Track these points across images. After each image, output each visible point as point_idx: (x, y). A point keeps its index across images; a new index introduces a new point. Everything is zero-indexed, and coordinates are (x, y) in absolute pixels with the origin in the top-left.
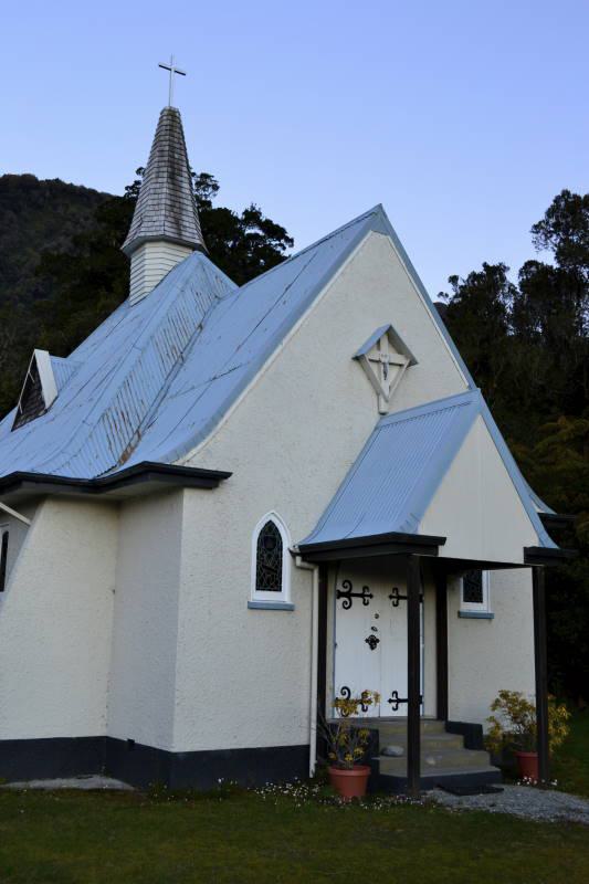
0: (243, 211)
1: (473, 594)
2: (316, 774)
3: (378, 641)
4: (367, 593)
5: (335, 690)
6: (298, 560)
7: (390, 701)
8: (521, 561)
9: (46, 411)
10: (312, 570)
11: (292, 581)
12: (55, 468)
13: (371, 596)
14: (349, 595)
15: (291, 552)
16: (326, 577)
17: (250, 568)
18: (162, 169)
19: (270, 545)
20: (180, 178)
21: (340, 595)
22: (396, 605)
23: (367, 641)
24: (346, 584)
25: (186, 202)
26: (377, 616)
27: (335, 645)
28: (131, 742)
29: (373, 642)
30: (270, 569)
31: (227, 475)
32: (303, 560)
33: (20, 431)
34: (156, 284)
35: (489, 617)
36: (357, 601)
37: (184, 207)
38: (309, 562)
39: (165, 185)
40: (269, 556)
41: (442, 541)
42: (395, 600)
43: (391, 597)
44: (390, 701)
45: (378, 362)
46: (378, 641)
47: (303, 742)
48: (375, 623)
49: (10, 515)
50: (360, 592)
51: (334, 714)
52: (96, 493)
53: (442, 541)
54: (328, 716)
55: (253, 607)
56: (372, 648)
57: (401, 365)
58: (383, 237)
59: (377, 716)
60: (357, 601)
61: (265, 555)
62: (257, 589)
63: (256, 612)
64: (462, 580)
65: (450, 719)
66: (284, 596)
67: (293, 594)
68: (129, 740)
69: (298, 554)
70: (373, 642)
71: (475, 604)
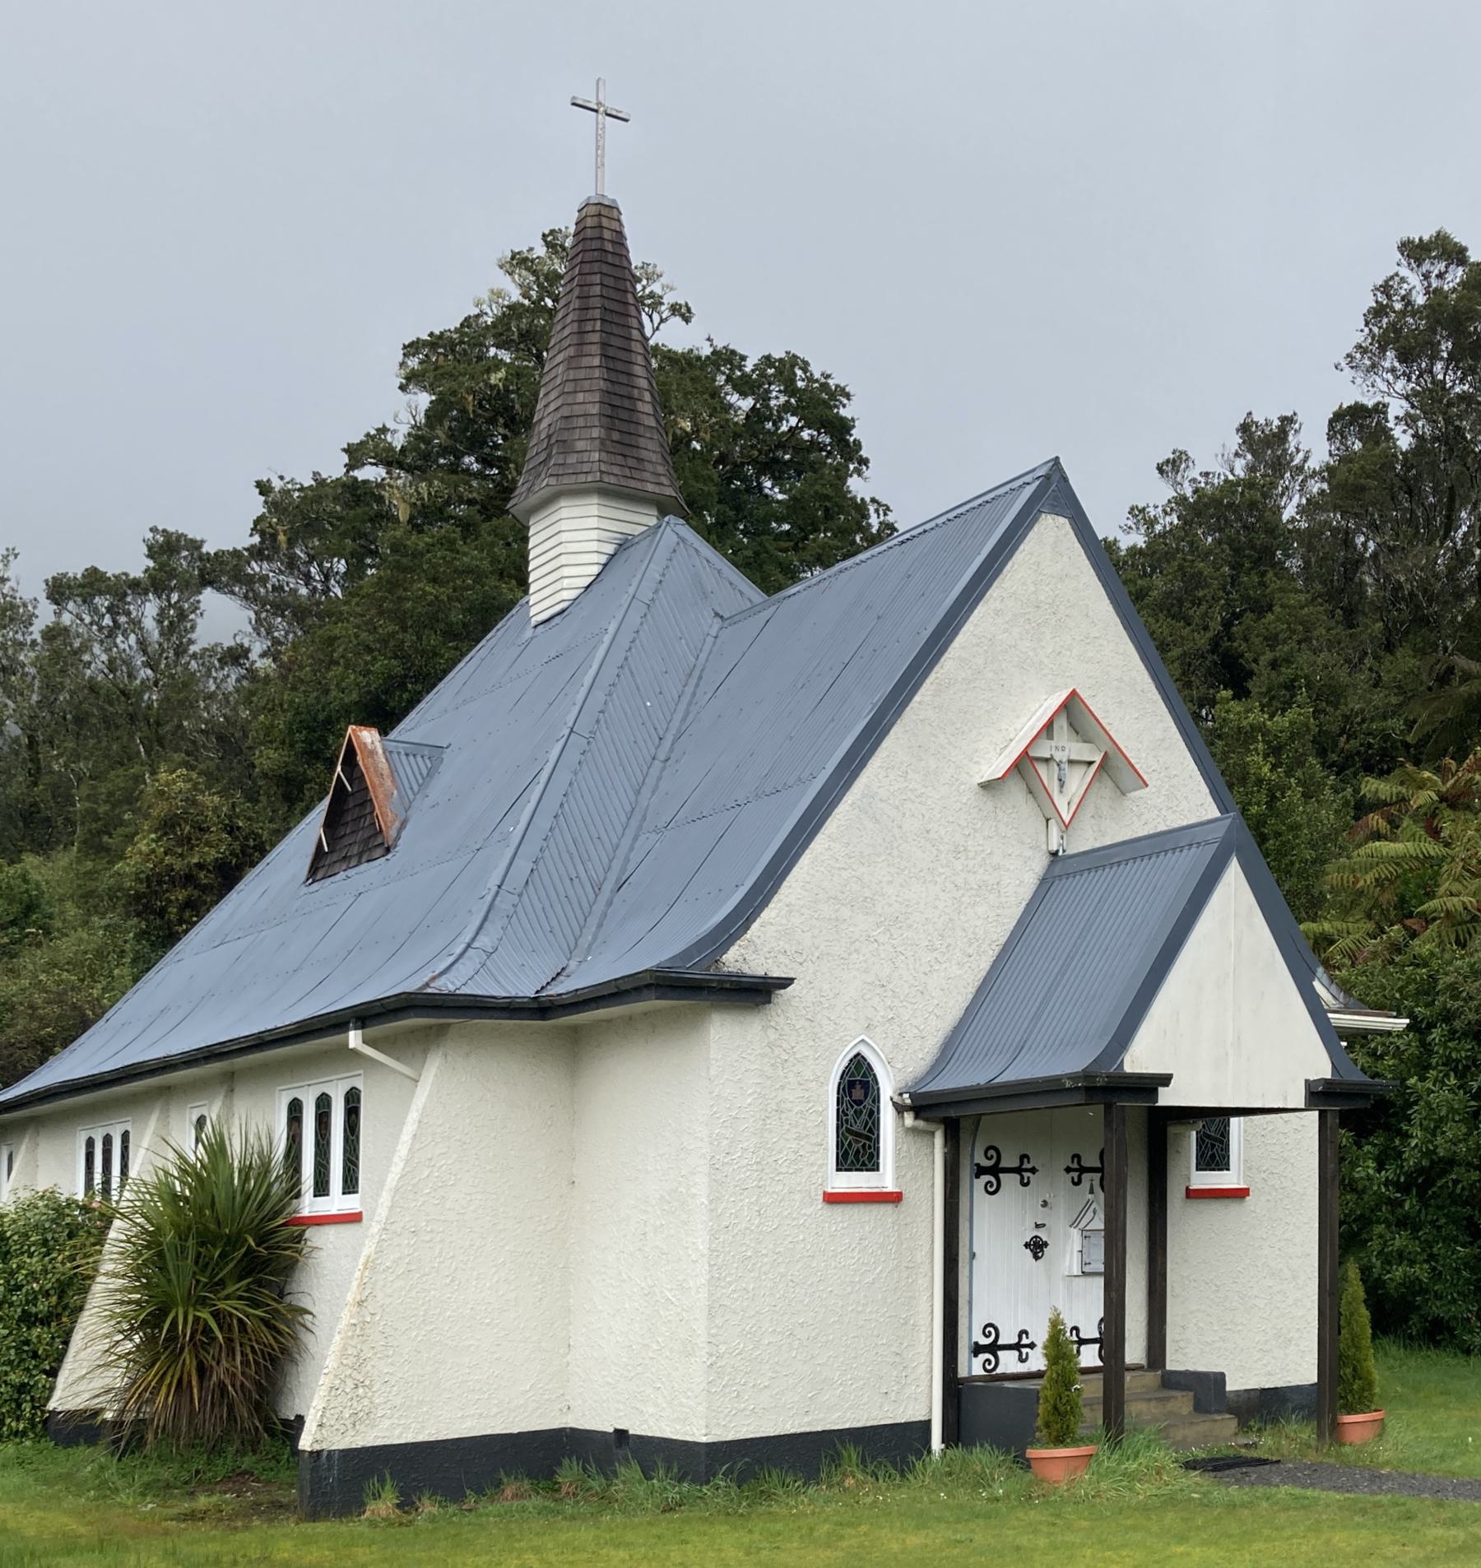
1: (1212, 1156)
3: (1046, 1244)
4: (1026, 1166)
5: (972, 1332)
6: (909, 1119)
7: (1032, 1346)
9: (388, 850)
10: (933, 1134)
11: (898, 1152)
12: (458, 984)
13: (1033, 1170)
14: (995, 1171)
15: (895, 1104)
16: (958, 1142)
17: (826, 1136)
19: (858, 1093)
21: (980, 1171)
22: (1077, 1183)
23: (1027, 1245)
24: (991, 1152)
26: (1045, 1204)
27: (973, 1256)
28: (621, 1434)
29: (1037, 1247)
31: (786, 982)
32: (916, 1117)
33: (326, 887)
34: (587, 581)
35: (1240, 1194)
36: (1009, 1181)
38: (926, 1120)
39: (597, 373)
40: (858, 1113)
41: (1165, 1080)
43: (1068, 1170)
46: (1046, 1244)
47: (918, 1415)
49: (382, 1064)
50: (1015, 1164)
51: (973, 1367)
52: (543, 1019)
53: (1165, 1080)
54: (962, 1372)
55: (832, 1199)
56: (1036, 1258)
57: (1090, 763)
60: (1009, 1181)
61: (851, 1112)
62: (838, 1170)
64: (1194, 1133)
65: (1170, 1366)
66: (885, 1179)
67: (898, 1177)
68: (617, 1431)
70: (1037, 1247)
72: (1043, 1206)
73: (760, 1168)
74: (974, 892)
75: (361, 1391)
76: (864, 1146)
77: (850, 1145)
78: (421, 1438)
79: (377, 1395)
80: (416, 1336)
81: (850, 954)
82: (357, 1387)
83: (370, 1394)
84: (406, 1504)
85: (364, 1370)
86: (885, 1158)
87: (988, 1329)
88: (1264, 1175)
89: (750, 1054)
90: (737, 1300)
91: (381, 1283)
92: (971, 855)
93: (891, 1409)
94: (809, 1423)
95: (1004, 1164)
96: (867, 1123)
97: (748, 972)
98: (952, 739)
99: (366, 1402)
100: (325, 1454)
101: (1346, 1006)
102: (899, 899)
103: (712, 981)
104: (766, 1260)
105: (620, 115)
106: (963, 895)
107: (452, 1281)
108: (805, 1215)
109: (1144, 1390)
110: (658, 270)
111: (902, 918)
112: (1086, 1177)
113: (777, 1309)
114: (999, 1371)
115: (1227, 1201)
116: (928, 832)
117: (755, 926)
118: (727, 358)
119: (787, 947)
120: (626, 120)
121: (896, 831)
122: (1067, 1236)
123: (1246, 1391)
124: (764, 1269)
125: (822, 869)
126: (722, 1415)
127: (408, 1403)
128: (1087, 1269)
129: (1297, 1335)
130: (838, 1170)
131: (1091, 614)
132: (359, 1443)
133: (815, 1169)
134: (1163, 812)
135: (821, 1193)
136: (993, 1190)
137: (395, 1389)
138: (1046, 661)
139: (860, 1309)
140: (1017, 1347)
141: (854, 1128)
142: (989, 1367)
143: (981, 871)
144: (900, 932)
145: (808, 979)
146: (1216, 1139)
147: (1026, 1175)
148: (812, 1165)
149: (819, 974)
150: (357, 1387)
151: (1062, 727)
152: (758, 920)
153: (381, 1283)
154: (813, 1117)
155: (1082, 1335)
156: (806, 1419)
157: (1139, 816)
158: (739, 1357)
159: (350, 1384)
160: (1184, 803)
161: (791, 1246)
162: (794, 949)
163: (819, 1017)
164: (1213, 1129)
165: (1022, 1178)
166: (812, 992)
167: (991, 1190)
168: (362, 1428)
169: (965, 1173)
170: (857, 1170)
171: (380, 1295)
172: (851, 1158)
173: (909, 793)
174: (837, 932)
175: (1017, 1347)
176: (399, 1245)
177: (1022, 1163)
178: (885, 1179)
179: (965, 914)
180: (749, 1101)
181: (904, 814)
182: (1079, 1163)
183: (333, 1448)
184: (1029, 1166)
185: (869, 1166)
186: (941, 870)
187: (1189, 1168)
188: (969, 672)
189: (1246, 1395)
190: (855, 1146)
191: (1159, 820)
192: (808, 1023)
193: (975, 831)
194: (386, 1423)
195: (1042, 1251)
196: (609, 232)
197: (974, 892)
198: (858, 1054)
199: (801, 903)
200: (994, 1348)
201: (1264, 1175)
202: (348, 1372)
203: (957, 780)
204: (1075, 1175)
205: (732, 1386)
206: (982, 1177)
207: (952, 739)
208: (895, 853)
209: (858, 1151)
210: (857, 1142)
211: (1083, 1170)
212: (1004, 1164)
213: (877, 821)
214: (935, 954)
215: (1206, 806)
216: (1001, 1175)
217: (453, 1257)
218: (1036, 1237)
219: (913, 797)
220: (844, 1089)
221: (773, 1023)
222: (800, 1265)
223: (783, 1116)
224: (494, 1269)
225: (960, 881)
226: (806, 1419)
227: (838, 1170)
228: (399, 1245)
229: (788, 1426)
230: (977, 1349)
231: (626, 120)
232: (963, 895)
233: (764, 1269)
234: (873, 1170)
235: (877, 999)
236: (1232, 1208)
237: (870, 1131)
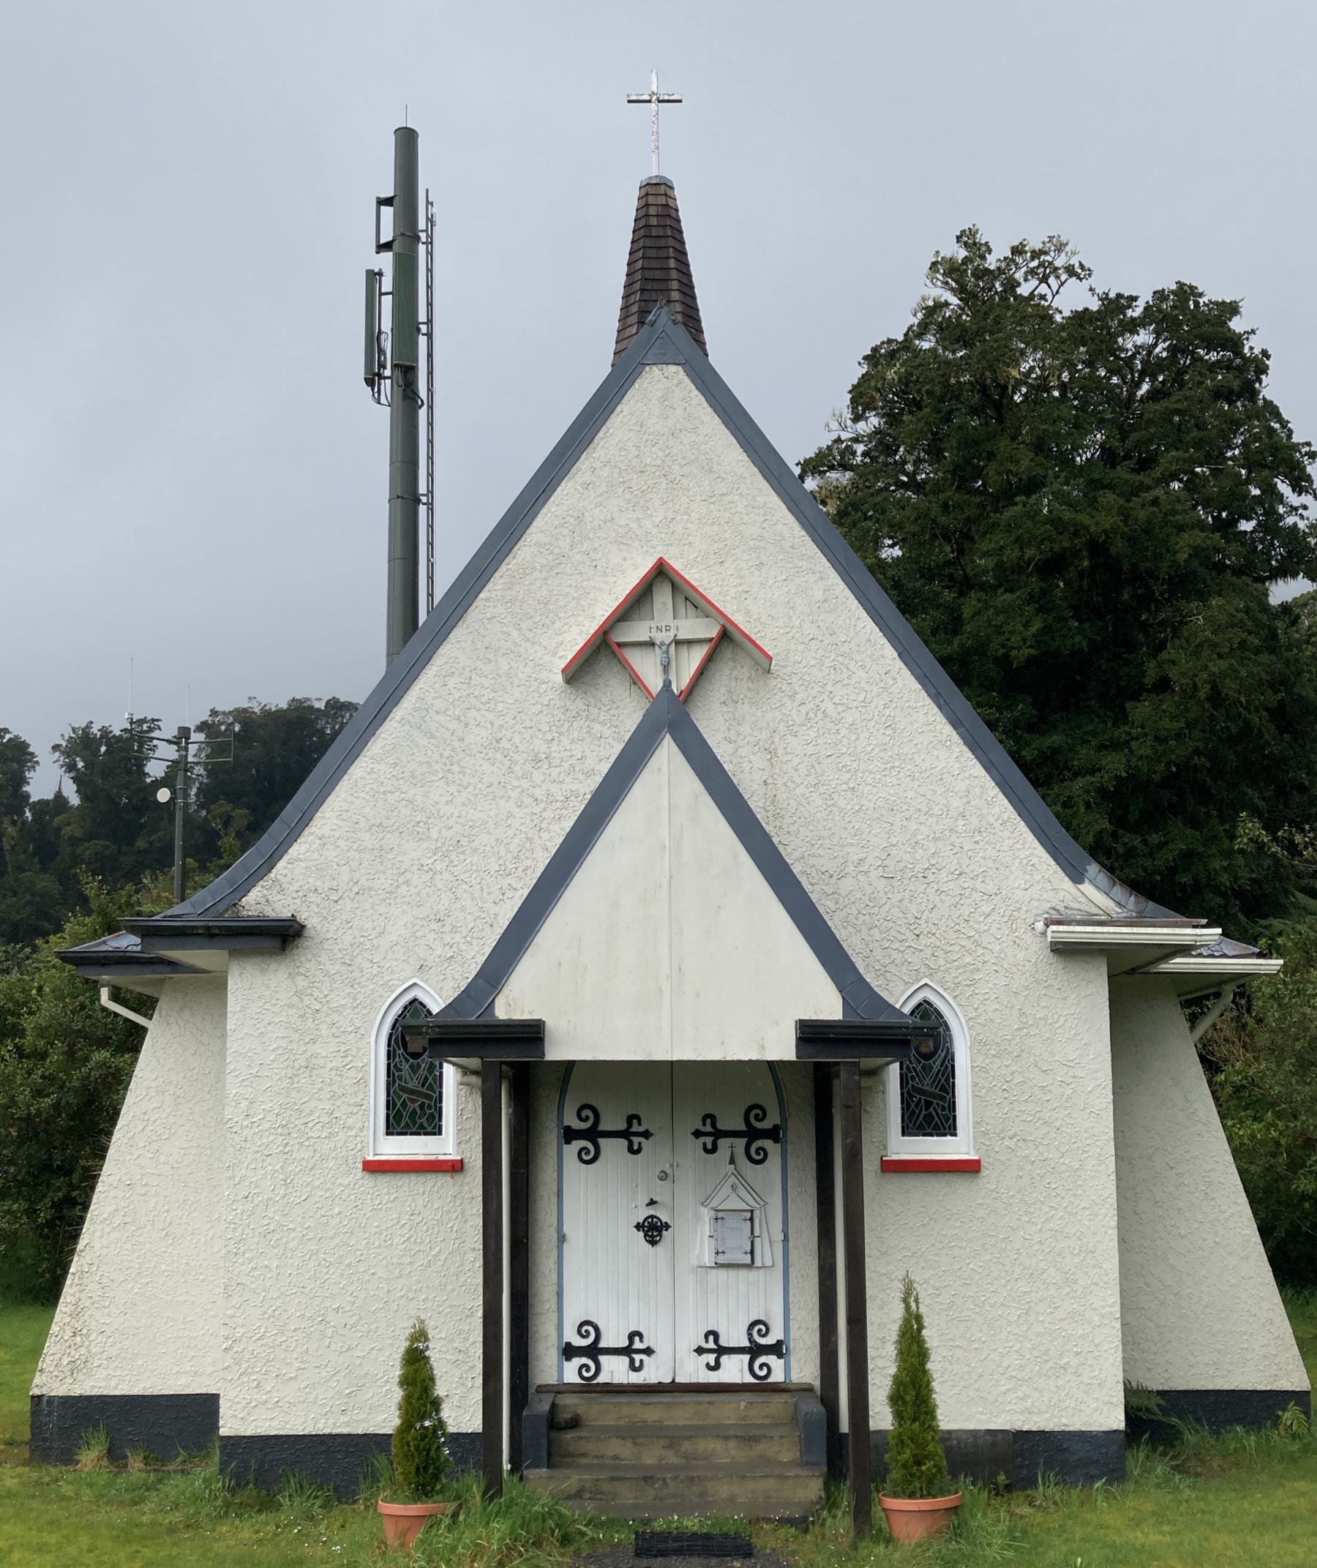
0: (1118, 291)
2: (1145, 1432)
4: (635, 1128)
7: (700, 1351)
13: (646, 1134)
14: (593, 1134)
21: (570, 1135)
22: (713, 1150)
23: (638, 1227)
24: (586, 1113)
27: (562, 1238)
29: (653, 1230)
30: (412, 1092)
35: (970, 1168)
36: (612, 1148)
43: (697, 1134)
44: (648, 1351)
45: (651, 644)
48: (661, 1194)
50: (622, 1126)
55: (375, 1168)
59: (668, 1380)
60: (612, 1148)
63: (385, 1183)
72: (661, 1179)
73: (286, 1131)
74: (559, 804)
75: (78, 1339)
76: (422, 1106)
77: (404, 1104)
78: (135, 1392)
79: (93, 1344)
80: (132, 1288)
81: (397, 887)
82: (75, 1335)
83: (87, 1343)
84: (115, 1455)
85: (82, 1319)
86: (447, 1122)
87: (585, 1328)
88: (1012, 1143)
89: (275, 1005)
90: (257, 1278)
91: (98, 1234)
92: (556, 762)
93: (454, 1415)
94: (347, 1424)
95: (605, 1126)
96: (426, 1079)
97: (272, 915)
98: (530, 635)
99: (83, 1351)
100: (45, 1399)
101: (1141, 914)
102: (462, 820)
103: (196, 927)
104: (293, 1235)
105: (671, 98)
106: (544, 809)
107: (167, 1235)
108: (340, 1185)
109: (768, 1421)
110: (1064, 239)
111: (464, 841)
112: (724, 1143)
113: (306, 1291)
114: (601, 1379)
115: (948, 1177)
116: (498, 741)
117: (281, 864)
118: (1115, 305)
119: (319, 883)
120: (680, 101)
121: (456, 744)
122: (697, 1217)
123: (989, 1432)
124: (290, 1245)
125: (362, 795)
126: (239, 1406)
127: (123, 1355)
128: (721, 1259)
129: (1075, 1361)
130: (388, 1134)
131: (715, 468)
132: (77, 1391)
133: (353, 1133)
134: (829, 688)
135: (360, 1160)
136: (589, 1159)
137: (111, 1340)
138: (654, 531)
139: (411, 1295)
140: (627, 1351)
141: (410, 1085)
142: (585, 1374)
143: (568, 780)
144: (462, 857)
145: (344, 918)
146: (933, 1095)
147: (636, 1140)
148: (350, 1128)
149: (358, 912)
150: (75, 1335)
151: (665, 604)
152: (286, 858)
153: (98, 1234)
154: (352, 1074)
155: (723, 1342)
156: (344, 1419)
157: (792, 697)
158: (260, 1343)
159: (69, 1332)
160: (861, 673)
161: (324, 1220)
162: (327, 886)
163: (359, 959)
164: (928, 1081)
165: (631, 1143)
166: (350, 932)
167: (586, 1158)
168: (80, 1377)
169: (550, 1137)
170: (412, 1134)
171: (97, 1245)
172: (405, 1119)
173: (474, 701)
174: (382, 863)
175: (627, 1351)
176: (115, 1197)
177: (630, 1125)
178: (444, 1146)
179: (548, 830)
180: (272, 1057)
181: (467, 725)
182: (713, 1125)
183: (52, 1394)
184: (641, 1129)
185: (429, 1130)
186: (516, 783)
187: (884, 1133)
188: (550, 558)
189: (989, 1438)
190: (411, 1106)
191: (824, 696)
192: (345, 967)
193: (561, 734)
194: (102, 1373)
195: (660, 1235)
196: (655, 208)
197: (559, 804)
198: (415, 1000)
199: (337, 834)
200: (594, 1351)
201: (1012, 1143)
202: (67, 1320)
203: (536, 680)
204: (709, 1140)
205: (252, 1374)
206: (574, 1143)
207: (530, 635)
208: (455, 768)
209: (414, 1112)
210: (413, 1101)
211: (718, 1134)
212: (605, 1126)
213: (433, 736)
214: (509, 880)
215: (894, 673)
216: (601, 1141)
217: (167, 1211)
218: (652, 1217)
219: (478, 705)
220: (396, 1039)
221: (301, 970)
222: (336, 1241)
223: (314, 1073)
224: (209, 1226)
225: (539, 793)
226: (344, 1419)
227: (388, 1134)
228: (115, 1197)
229: (321, 1426)
230: (569, 1352)
231: (680, 101)
232: (544, 809)
233: (290, 1245)
234: (434, 1134)
235: (431, 936)
236: (959, 1186)
237: (430, 1088)
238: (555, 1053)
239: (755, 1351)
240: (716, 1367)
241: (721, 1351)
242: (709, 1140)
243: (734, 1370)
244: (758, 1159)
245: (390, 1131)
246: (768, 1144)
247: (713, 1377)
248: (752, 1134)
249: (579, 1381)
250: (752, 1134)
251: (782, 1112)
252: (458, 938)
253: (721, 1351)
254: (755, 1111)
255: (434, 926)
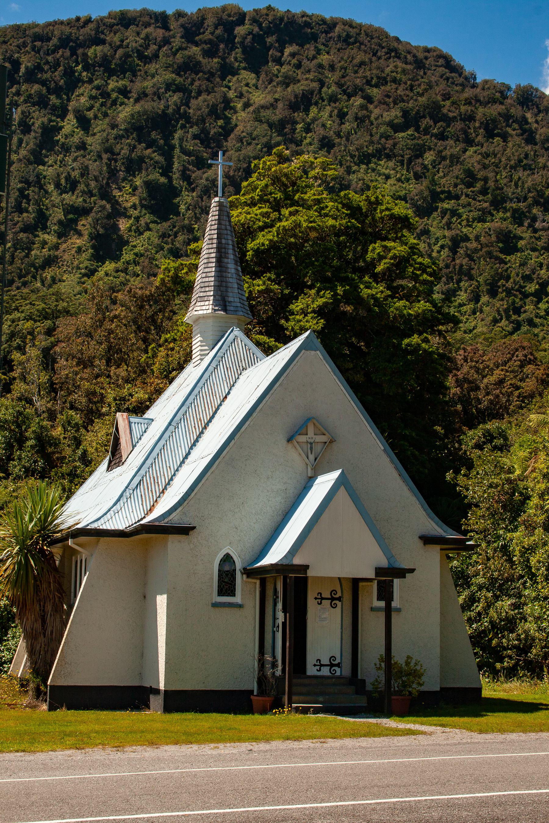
7: (315, 665)
8: (373, 576)
9: (123, 464)
18: (211, 260)
20: (226, 260)
25: (231, 280)
31: (194, 528)
35: (240, 606)
37: (230, 285)
42: (319, 600)
44: (315, 665)
55: (215, 605)
58: (313, 353)
63: (217, 610)
66: (237, 599)
69: (244, 574)
71: (232, 598)
155: (322, 663)
238: (310, 573)
239: (331, 665)
240: (320, 670)
241: (321, 665)
242: (319, 600)
243: (325, 672)
244: (334, 607)
245: (219, 595)
246: (337, 602)
247: (319, 674)
248: (332, 599)
249: (329, 674)
250: (332, 599)
251: (342, 592)
252: (242, 534)
253: (321, 665)
254: (333, 592)
255: (235, 529)
